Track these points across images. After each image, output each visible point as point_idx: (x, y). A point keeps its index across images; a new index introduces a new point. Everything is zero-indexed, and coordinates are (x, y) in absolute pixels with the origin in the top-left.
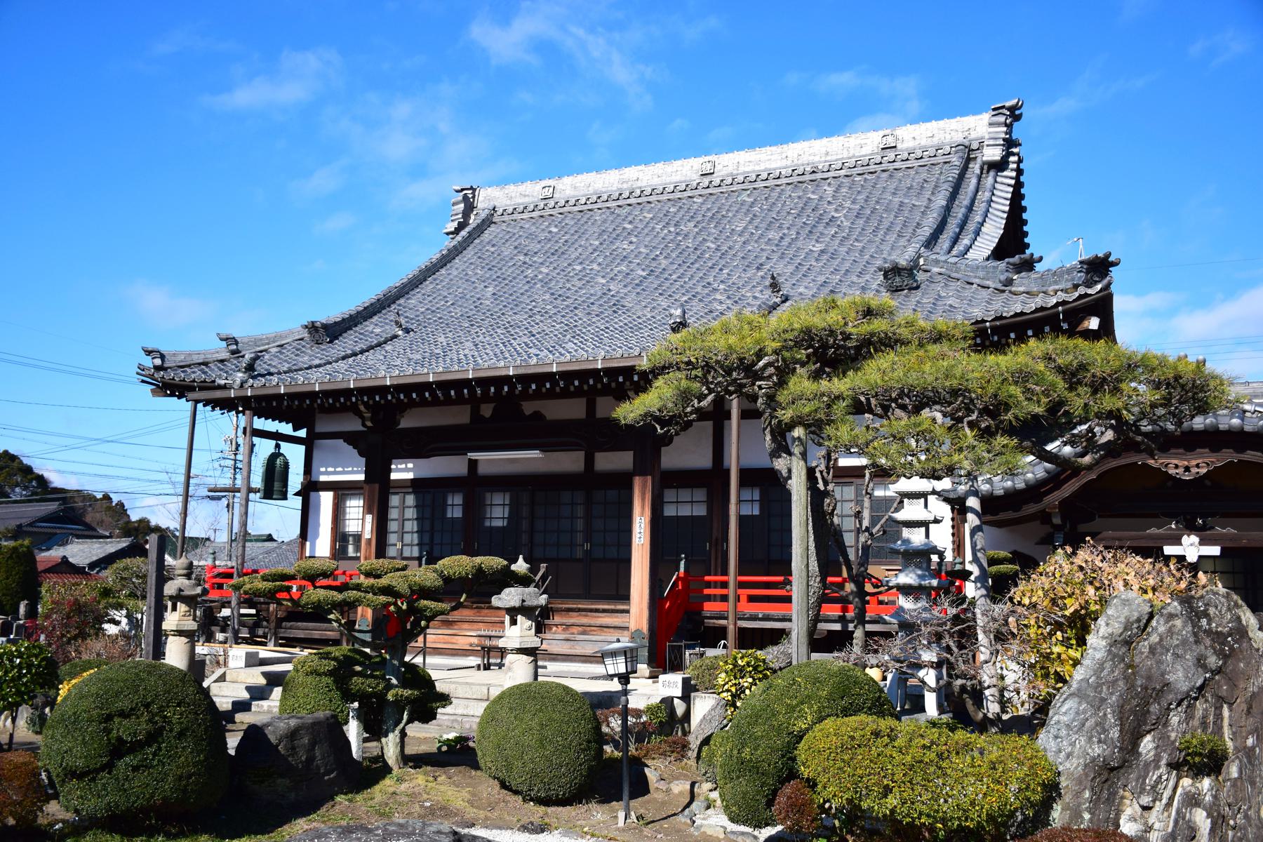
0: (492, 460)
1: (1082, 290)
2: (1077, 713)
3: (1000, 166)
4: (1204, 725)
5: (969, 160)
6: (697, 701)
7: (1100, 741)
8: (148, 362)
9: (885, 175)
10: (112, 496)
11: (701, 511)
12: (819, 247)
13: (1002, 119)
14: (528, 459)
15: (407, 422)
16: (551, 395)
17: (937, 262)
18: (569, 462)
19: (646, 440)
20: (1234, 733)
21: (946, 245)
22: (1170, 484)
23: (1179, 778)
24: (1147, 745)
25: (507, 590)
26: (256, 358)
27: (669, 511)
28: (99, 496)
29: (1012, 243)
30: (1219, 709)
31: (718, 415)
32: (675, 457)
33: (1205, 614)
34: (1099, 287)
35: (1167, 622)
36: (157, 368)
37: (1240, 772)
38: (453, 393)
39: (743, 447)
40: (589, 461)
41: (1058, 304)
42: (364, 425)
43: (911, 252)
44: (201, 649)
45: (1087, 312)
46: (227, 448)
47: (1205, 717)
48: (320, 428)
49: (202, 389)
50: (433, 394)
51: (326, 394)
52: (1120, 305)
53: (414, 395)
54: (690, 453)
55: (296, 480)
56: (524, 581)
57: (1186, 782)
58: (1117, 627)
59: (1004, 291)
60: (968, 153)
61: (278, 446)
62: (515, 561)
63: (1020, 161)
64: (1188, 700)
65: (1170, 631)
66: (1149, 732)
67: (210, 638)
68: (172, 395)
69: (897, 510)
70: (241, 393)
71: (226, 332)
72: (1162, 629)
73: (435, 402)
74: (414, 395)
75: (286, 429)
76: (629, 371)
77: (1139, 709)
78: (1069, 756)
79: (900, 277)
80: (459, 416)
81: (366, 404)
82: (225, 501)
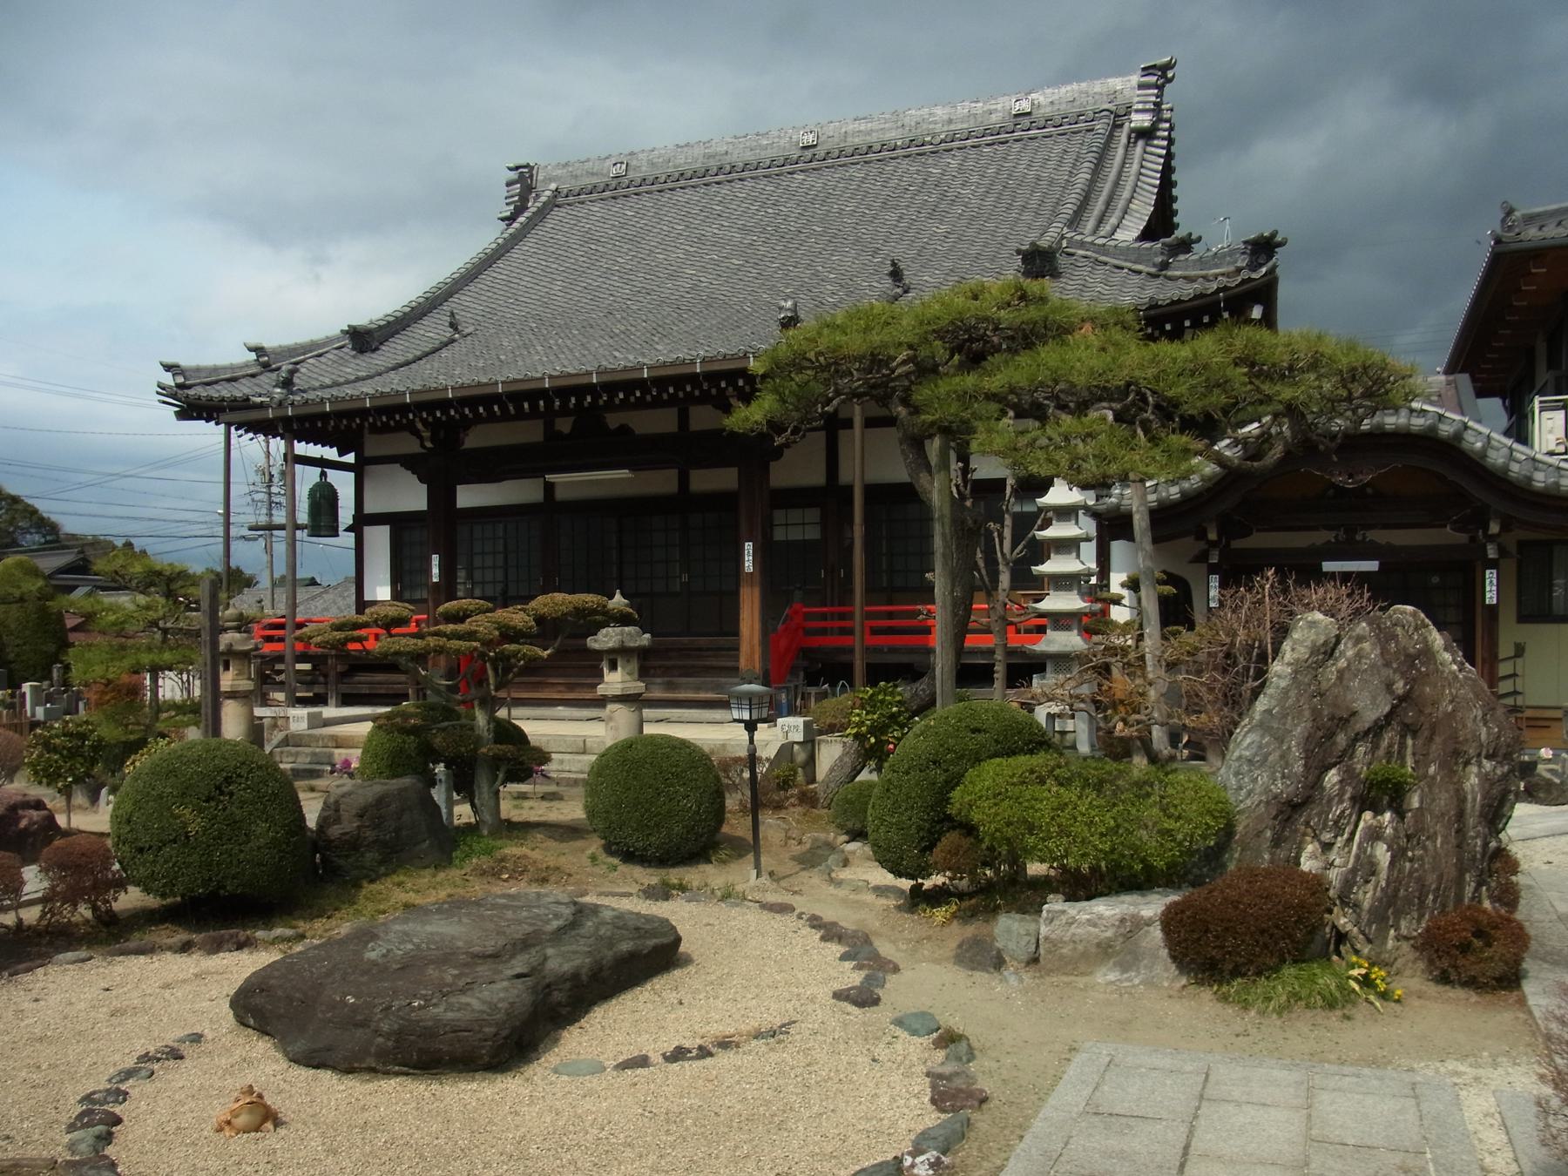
0: (571, 483)
1: (1245, 275)
2: (1260, 747)
3: (1146, 134)
4: (1389, 754)
5: (1117, 126)
6: (823, 746)
7: (1283, 777)
8: (168, 379)
9: (1018, 145)
10: (133, 540)
11: (813, 533)
12: (943, 228)
13: (1153, 79)
14: (613, 479)
15: (475, 439)
16: (641, 404)
17: (1082, 245)
18: (662, 482)
19: (754, 451)
20: (1416, 762)
21: (1090, 225)
22: (1331, 492)
23: (1361, 812)
24: (1332, 777)
25: (604, 631)
26: (292, 372)
27: (779, 535)
28: (119, 543)
29: (1161, 223)
30: (1403, 737)
31: (835, 425)
32: (783, 475)
33: (1395, 637)
34: (1264, 270)
35: (1355, 645)
36: (179, 386)
37: (1421, 802)
38: (526, 405)
39: (873, 461)
40: (684, 480)
41: (1219, 290)
42: (423, 446)
43: (1053, 233)
44: (259, 712)
45: (1250, 296)
46: (258, 479)
47: (1390, 746)
48: (369, 451)
49: (232, 409)
50: (504, 408)
51: (379, 411)
52: (1284, 292)
53: (481, 410)
54: (799, 468)
55: (346, 515)
56: (623, 620)
57: (1368, 815)
58: (1303, 652)
59: (1157, 276)
60: (1117, 118)
61: (323, 474)
62: (611, 597)
63: (1171, 129)
64: (1377, 729)
65: (1359, 656)
66: (1334, 765)
67: (265, 702)
68: (199, 418)
69: (1042, 528)
70: (280, 413)
71: (254, 342)
72: (1350, 653)
73: (505, 417)
74: (481, 410)
75: (331, 453)
76: (732, 375)
77: (1327, 737)
78: (1249, 793)
79: (1040, 262)
80: (529, 433)
81: (424, 422)
82: (262, 542)
